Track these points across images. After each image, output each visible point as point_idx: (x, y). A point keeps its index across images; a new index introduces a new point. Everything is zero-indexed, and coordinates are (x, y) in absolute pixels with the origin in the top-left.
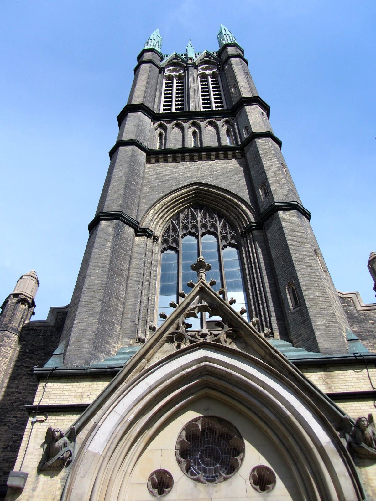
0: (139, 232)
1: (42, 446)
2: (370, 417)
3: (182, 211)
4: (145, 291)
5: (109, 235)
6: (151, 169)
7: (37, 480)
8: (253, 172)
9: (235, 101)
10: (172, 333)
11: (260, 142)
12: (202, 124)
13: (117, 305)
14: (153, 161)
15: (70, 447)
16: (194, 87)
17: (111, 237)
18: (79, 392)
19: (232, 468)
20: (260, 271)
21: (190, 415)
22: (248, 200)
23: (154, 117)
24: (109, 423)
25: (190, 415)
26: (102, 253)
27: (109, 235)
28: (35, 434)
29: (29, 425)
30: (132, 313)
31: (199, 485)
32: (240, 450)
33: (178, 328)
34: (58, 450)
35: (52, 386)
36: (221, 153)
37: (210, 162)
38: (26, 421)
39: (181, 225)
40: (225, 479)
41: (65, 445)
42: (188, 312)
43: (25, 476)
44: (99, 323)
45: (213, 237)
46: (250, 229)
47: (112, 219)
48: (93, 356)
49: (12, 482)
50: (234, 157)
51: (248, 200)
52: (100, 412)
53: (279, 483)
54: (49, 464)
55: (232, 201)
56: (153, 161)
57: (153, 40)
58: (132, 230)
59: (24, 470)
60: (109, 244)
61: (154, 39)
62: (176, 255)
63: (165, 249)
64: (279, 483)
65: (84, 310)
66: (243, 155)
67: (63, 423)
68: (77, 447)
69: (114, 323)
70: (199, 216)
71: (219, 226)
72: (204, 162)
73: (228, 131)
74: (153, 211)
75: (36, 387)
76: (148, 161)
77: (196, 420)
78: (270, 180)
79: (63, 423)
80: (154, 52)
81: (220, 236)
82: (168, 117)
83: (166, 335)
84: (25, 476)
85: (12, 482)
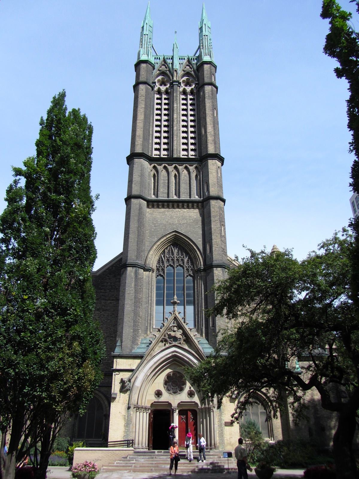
0: (145, 270)
1: (120, 383)
2: (350, 14)
3: (166, 248)
4: (150, 306)
5: (132, 278)
6: (151, 214)
7: (120, 395)
8: (206, 228)
9: (204, 154)
10: (163, 339)
11: (213, 202)
12: (180, 168)
13: (139, 320)
14: (150, 207)
15: (129, 385)
16: (177, 107)
17: (134, 280)
18: (130, 363)
19: (182, 390)
20: (202, 299)
21: (169, 371)
22: (201, 248)
23: (151, 160)
24: (141, 376)
25: (169, 371)
26: (130, 291)
27: (132, 278)
28: (117, 379)
29: (114, 376)
30: (145, 320)
31: (171, 395)
32: (185, 384)
33: (165, 336)
34: (126, 386)
35: (119, 361)
36: (190, 204)
37: (184, 210)
38: (112, 374)
39: (166, 258)
40: (179, 393)
41: (128, 384)
42: (205, 467)
43: (116, 394)
44: (133, 332)
45: (181, 268)
46: (199, 270)
47: (133, 267)
48: (133, 348)
49: (113, 396)
50: (198, 207)
51: (202, 251)
52: (138, 372)
53: (196, 395)
54: (123, 390)
55: (193, 247)
56: (150, 207)
57: (146, 35)
58: (142, 270)
59: (115, 392)
60: (133, 285)
61: (147, 35)
62: (163, 280)
63: (158, 276)
64: (196, 395)
65: (126, 324)
66: (203, 207)
67: (126, 376)
68: (132, 384)
69: (139, 329)
70: (176, 251)
71: (186, 260)
72: (180, 210)
73: (196, 176)
74: (151, 253)
75: (113, 362)
76: (148, 207)
77: (170, 372)
78: (214, 241)
79: (126, 376)
80: (148, 64)
81: (185, 268)
82: (159, 160)
83: (160, 340)
84: (116, 394)
85: (113, 396)
